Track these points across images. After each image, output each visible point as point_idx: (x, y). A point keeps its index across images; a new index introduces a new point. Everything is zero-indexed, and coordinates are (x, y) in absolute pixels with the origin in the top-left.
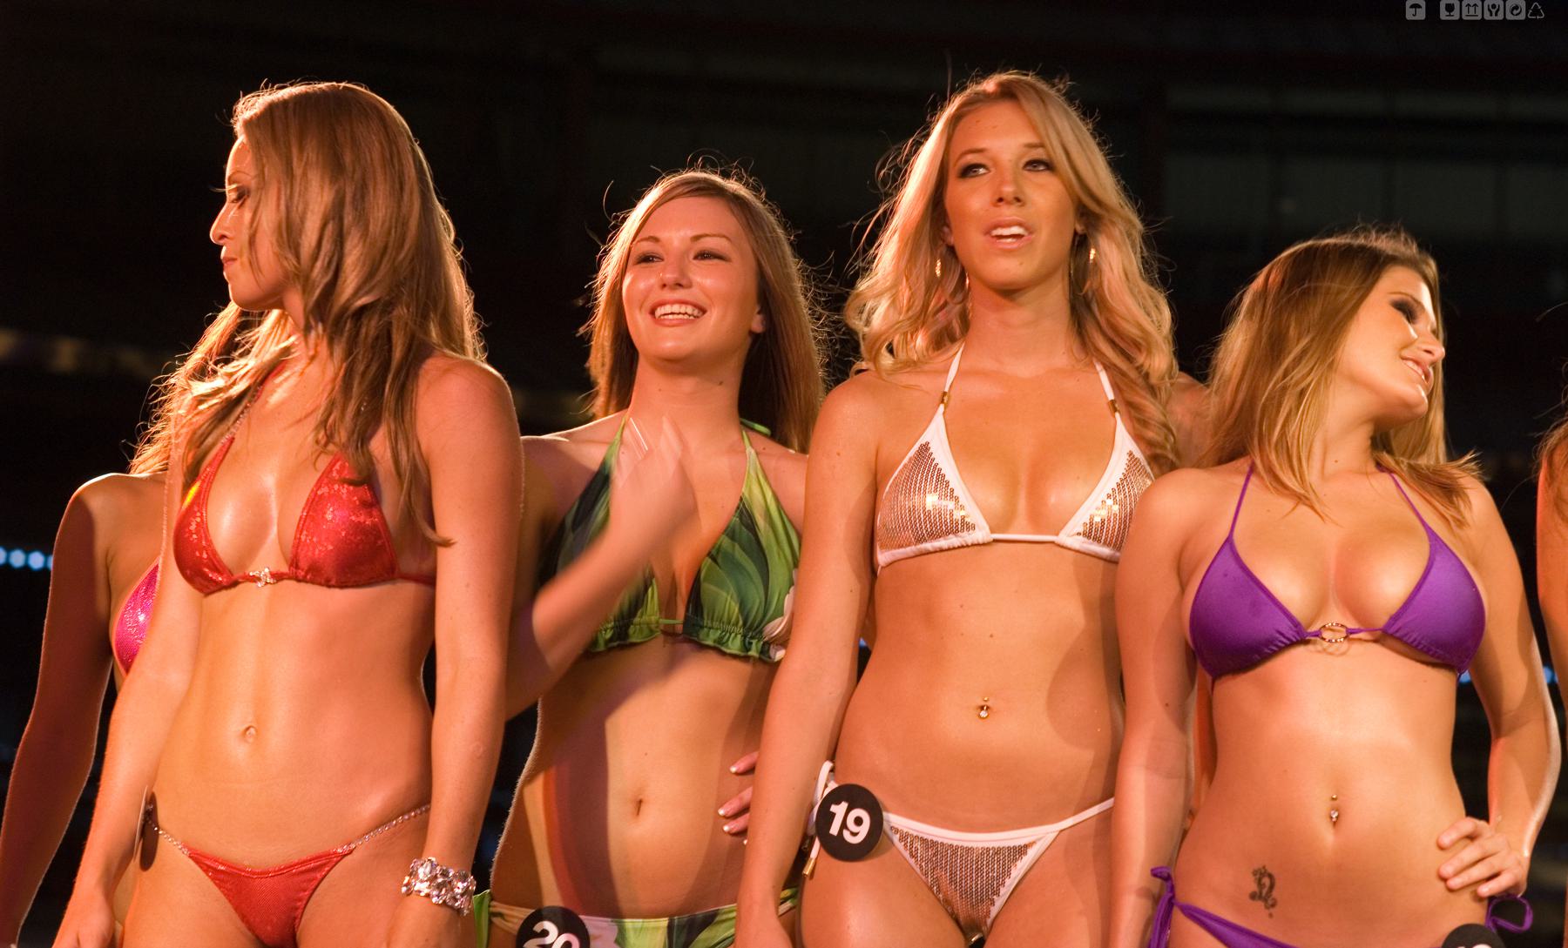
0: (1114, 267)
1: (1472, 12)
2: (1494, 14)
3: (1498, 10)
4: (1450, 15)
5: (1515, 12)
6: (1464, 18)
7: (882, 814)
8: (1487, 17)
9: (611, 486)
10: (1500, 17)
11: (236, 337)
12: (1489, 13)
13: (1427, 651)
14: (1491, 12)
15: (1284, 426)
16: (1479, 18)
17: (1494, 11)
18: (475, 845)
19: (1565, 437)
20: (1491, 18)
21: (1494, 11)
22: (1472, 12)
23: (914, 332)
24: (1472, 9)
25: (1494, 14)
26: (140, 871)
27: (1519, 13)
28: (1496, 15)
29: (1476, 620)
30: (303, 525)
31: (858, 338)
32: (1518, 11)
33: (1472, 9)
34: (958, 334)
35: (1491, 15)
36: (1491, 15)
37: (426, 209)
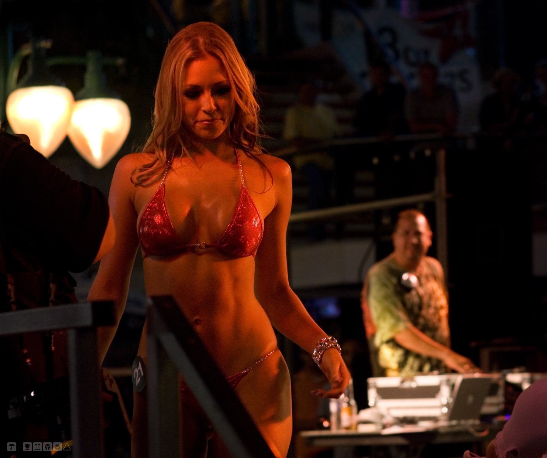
1: (37, 448)
2: (48, 448)
3: (50, 447)
4: (27, 449)
6: (34, 450)
8: (45, 450)
9: (439, 393)
11: (157, 209)
12: (45, 448)
13: (276, 206)
16: (41, 450)
17: (48, 447)
21: (48, 447)
22: (37, 448)
24: (37, 446)
25: (48, 448)
26: (338, 399)
27: (60, 448)
28: (49, 449)
29: (253, 132)
33: (37, 446)
34: (201, 43)
35: (46, 449)
37: (155, 130)
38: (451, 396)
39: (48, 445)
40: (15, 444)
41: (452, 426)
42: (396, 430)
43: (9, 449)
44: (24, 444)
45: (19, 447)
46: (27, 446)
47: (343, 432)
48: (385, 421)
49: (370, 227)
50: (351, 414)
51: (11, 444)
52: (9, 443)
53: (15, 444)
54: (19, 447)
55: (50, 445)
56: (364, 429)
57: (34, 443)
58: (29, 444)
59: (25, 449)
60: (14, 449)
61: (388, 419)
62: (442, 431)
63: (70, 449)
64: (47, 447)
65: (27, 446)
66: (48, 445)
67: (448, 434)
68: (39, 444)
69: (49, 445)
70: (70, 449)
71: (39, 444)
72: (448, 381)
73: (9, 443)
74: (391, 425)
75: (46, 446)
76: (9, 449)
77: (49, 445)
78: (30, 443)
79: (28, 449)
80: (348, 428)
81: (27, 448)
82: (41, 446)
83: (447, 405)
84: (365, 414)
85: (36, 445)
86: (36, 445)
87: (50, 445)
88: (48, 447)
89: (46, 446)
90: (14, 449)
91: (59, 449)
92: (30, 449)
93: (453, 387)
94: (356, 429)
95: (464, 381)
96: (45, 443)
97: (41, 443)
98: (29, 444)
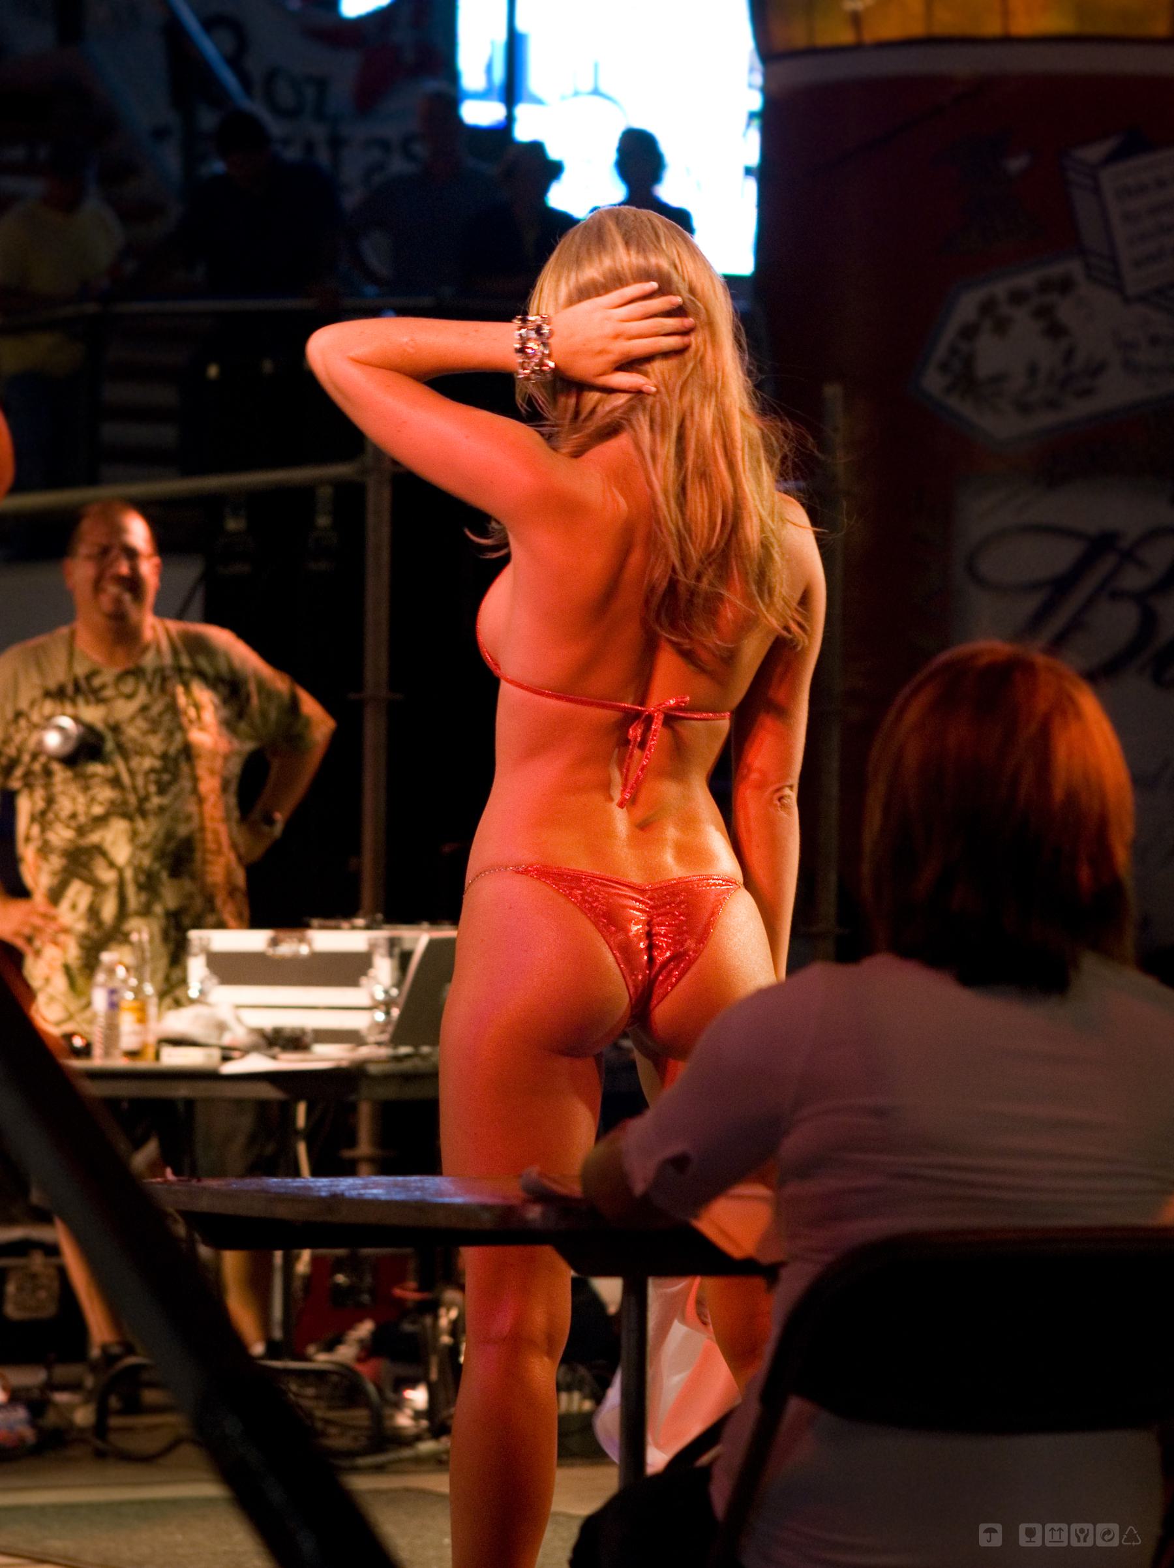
0: (754, 528)
1: (1056, 1538)
2: (1082, 1539)
3: (1087, 1535)
4: (1030, 1541)
5: (1107, 1537)
6: (1048, 1544)
7: (451, 1490)
10: (1089, 1543)
14: (1078, 1537)
15: (175, 1503)
16: (1065, 1544)
17: (1082, 1536)
18: (721, 1414)
19: (65, 1565)
20: (1079, 1545)
21: (1082, 1536)
22: (1056, 1538)
23: (800, 651)
24: (1056, 1534)
25: (1082, 1539)
28: (1085, 1541)
30: (601, 884)
31: (748, 351)
32: (1110, 1536)
33: (1056, 1534)
35: (1079, 1541)
36: (1079, 1541)
38: (399, 984)
39: (1082, 1531)
40: (998, 1527)
41: (397, 1059)
42: (257, 1063)
43: (983, 1540)
44: (1023, 1527)
45: (1010, 1535)
46: (1030, 1533)
47: (120, 1062)
48: (227, 1039)
49: (164, 395)
50: (142, 1020)
51: (989, 1529)
52: (983, 1527)
53: (998, 1527)
54: (1010, 1535)
55: (1088, 1530)
56: (174, 1058)
57: (1048, 1526)
58: (1034, 1528)
59: (1023, 1541)
60: (997, 1541)
61: (237, 1035)
62: (373, 1069)
63: (1138, 1541)
64: (1079, 1534)
65: (1030, 1533)
66: (1082, 1531)
67: (387, 1077)
68: (1060, 1529)
69: (1086, 1532)
70: (1138, 1541)
71: (1060, 1529)
72: (393, 943)
73: (983, 1527)
74: (246, 1051)
75: (1078, 1532)
76: (983, 1540)
77: (1086, 1532)
78: (1038, 1527)
79: (1032, 1539)
80: (133, 1054)
81: (1029, 1539)
82: (1065, 1535)
83: (387, 1005)
84: (178, 1022)
85: (1052, 1529)
86: (1052, 1529)
87: (1088, 1530)
88: (1084, 1534)
89: (1078, 1532)
90: (997, 1541)
91: (1109, 1540)
92: (1037, 1542)
93: (404, 959)
94: (157, 1056)
95: (432, 944)
96: (1075, 1527)
97: (1064, 1526)
98: (1034, 1528)
